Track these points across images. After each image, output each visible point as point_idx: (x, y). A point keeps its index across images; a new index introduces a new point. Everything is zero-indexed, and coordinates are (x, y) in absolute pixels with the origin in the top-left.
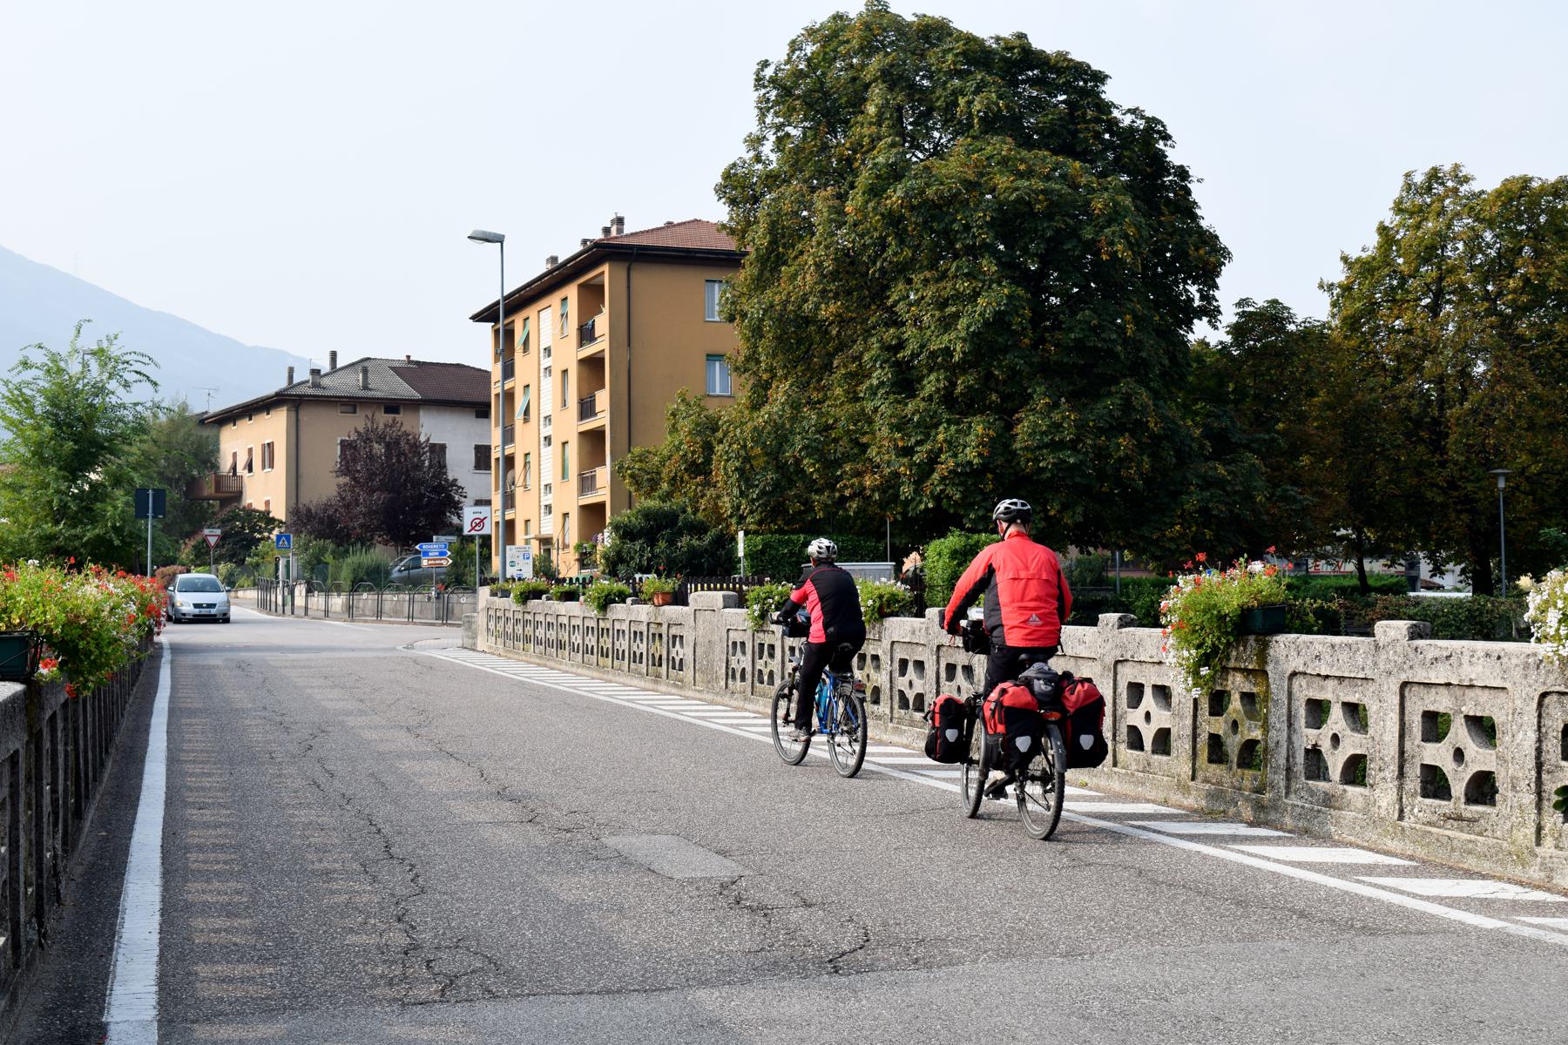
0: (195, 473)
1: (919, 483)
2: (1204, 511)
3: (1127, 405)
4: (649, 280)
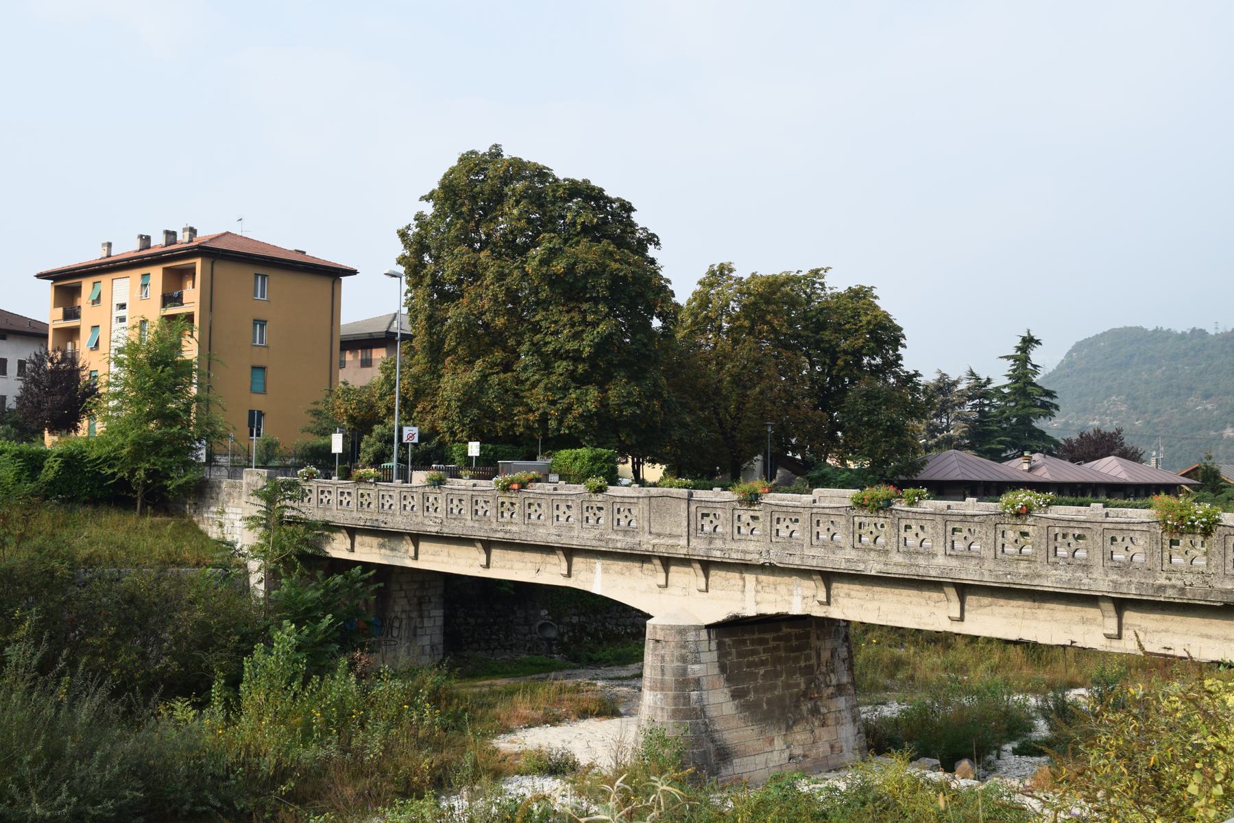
0: (536, 425)
1: (560, 422)
2: (681, 440)
3: (655, 385)
4: (226, 272)
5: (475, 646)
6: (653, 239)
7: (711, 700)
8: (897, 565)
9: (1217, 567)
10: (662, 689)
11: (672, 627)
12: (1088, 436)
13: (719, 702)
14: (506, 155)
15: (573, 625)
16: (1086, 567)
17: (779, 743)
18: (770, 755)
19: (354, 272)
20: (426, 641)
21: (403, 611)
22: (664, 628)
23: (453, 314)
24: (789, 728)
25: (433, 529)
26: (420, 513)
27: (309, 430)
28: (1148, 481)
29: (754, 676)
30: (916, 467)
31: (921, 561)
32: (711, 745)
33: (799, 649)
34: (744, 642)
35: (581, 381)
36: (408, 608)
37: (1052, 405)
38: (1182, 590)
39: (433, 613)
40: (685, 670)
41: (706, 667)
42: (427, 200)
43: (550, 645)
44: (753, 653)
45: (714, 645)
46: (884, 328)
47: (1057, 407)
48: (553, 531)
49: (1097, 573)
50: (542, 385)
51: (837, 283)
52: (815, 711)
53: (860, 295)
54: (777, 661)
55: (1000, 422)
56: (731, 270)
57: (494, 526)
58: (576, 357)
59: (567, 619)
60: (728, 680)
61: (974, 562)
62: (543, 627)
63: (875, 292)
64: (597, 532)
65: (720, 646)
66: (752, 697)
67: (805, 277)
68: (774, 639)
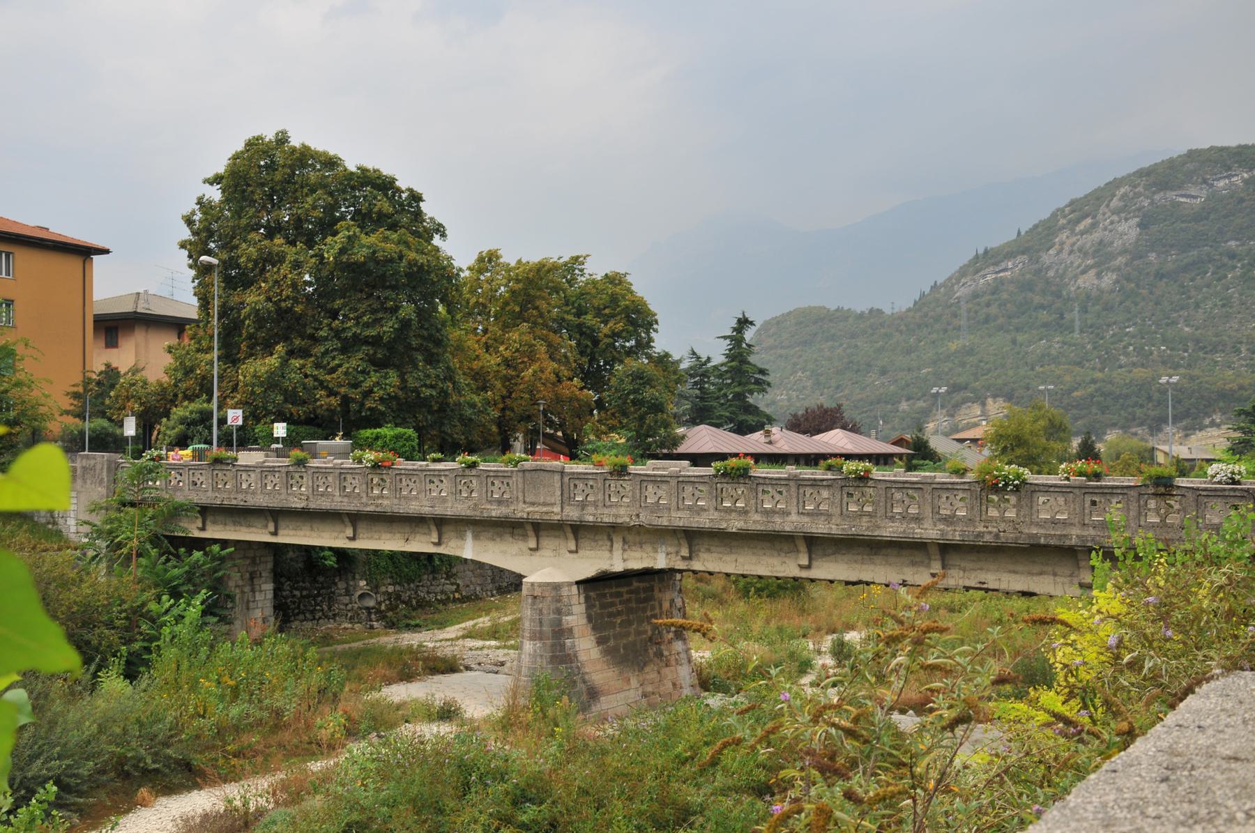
5: (301, 617)
6: (440, 230)
7: (582, 647)
8: (755, 522)
9: (1024, 516)
10: (541, 639)
11: (548, 584)
12: (813, 412)
13: (585, 646)
14: (295, 142)
15: (389, 594)
16: (918, 519)
17: (634, 682)
18: (627, 693)
19: (106, 252)
20: (258, 614)
21: (237, 586)
22: (541, 585)
23: (253, 299)
24: (641, 669)
25: (298, 504)
26: (284, 491)
27: (67, 412)
28: (807, 451)
29: (613, 625)
30: (677, 441)
31: (777, 519)
32: (583, 685)
33: (646, 600)
34: (604, 596)
35: (381, 365)
36: (240, 583)
37: (764, 382)
38: (997, 536)
39: (264, 587)
40: (560, 621)
41: (576, 618)
42: (211, 184)
43: (370, 613)
44: (612, 604)
45: (582, 600)
46: (638, 312)
47: (769, 384)
48: (427, 503)
49: (927, 524)
50: (343, 369)
51: (596, 269)
52: (660, 655)
53: (614, 280)
54: (630, 611)
55: (718, 398)
56: (498, 258)
57: (364, 500)
58: (376, 341)
59: (383, 589)
60: (594, 629)
61: (823, 518)
62: (362, 596)
63: (629, 278)
64: (471, 503)
65: (587, 599)
66: (612, 643)
67: (566, 264)
68: (628, 592)
